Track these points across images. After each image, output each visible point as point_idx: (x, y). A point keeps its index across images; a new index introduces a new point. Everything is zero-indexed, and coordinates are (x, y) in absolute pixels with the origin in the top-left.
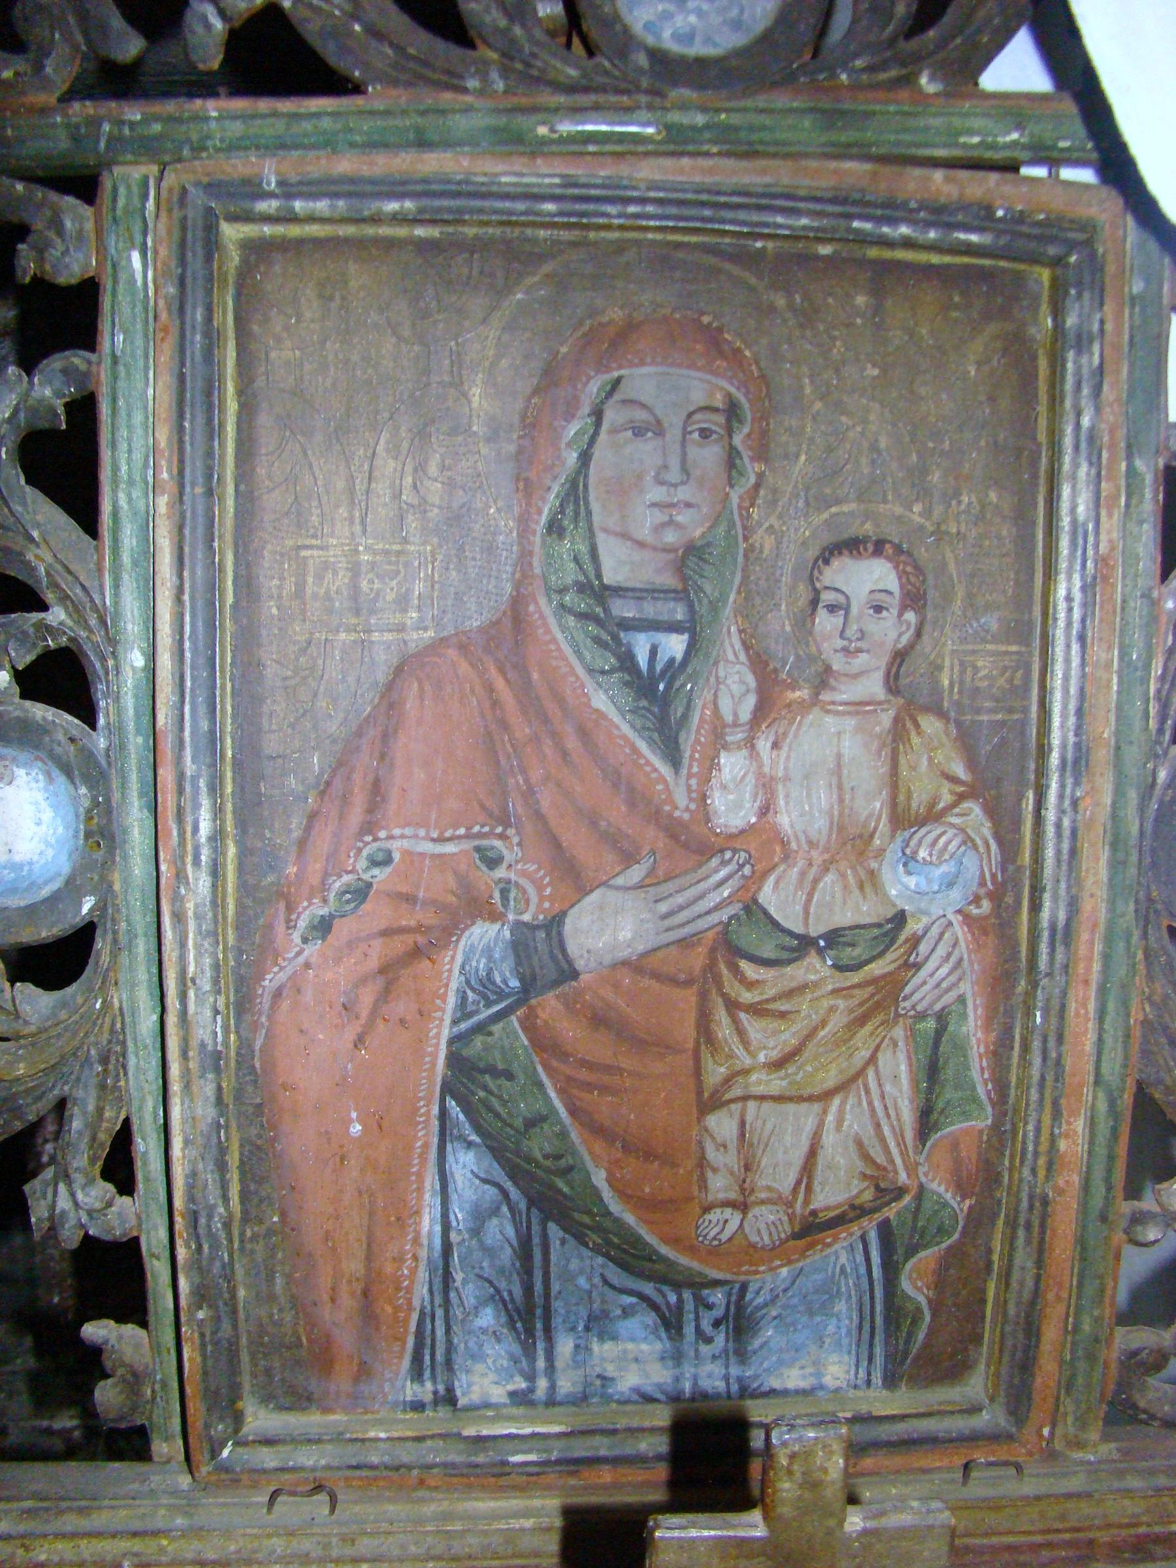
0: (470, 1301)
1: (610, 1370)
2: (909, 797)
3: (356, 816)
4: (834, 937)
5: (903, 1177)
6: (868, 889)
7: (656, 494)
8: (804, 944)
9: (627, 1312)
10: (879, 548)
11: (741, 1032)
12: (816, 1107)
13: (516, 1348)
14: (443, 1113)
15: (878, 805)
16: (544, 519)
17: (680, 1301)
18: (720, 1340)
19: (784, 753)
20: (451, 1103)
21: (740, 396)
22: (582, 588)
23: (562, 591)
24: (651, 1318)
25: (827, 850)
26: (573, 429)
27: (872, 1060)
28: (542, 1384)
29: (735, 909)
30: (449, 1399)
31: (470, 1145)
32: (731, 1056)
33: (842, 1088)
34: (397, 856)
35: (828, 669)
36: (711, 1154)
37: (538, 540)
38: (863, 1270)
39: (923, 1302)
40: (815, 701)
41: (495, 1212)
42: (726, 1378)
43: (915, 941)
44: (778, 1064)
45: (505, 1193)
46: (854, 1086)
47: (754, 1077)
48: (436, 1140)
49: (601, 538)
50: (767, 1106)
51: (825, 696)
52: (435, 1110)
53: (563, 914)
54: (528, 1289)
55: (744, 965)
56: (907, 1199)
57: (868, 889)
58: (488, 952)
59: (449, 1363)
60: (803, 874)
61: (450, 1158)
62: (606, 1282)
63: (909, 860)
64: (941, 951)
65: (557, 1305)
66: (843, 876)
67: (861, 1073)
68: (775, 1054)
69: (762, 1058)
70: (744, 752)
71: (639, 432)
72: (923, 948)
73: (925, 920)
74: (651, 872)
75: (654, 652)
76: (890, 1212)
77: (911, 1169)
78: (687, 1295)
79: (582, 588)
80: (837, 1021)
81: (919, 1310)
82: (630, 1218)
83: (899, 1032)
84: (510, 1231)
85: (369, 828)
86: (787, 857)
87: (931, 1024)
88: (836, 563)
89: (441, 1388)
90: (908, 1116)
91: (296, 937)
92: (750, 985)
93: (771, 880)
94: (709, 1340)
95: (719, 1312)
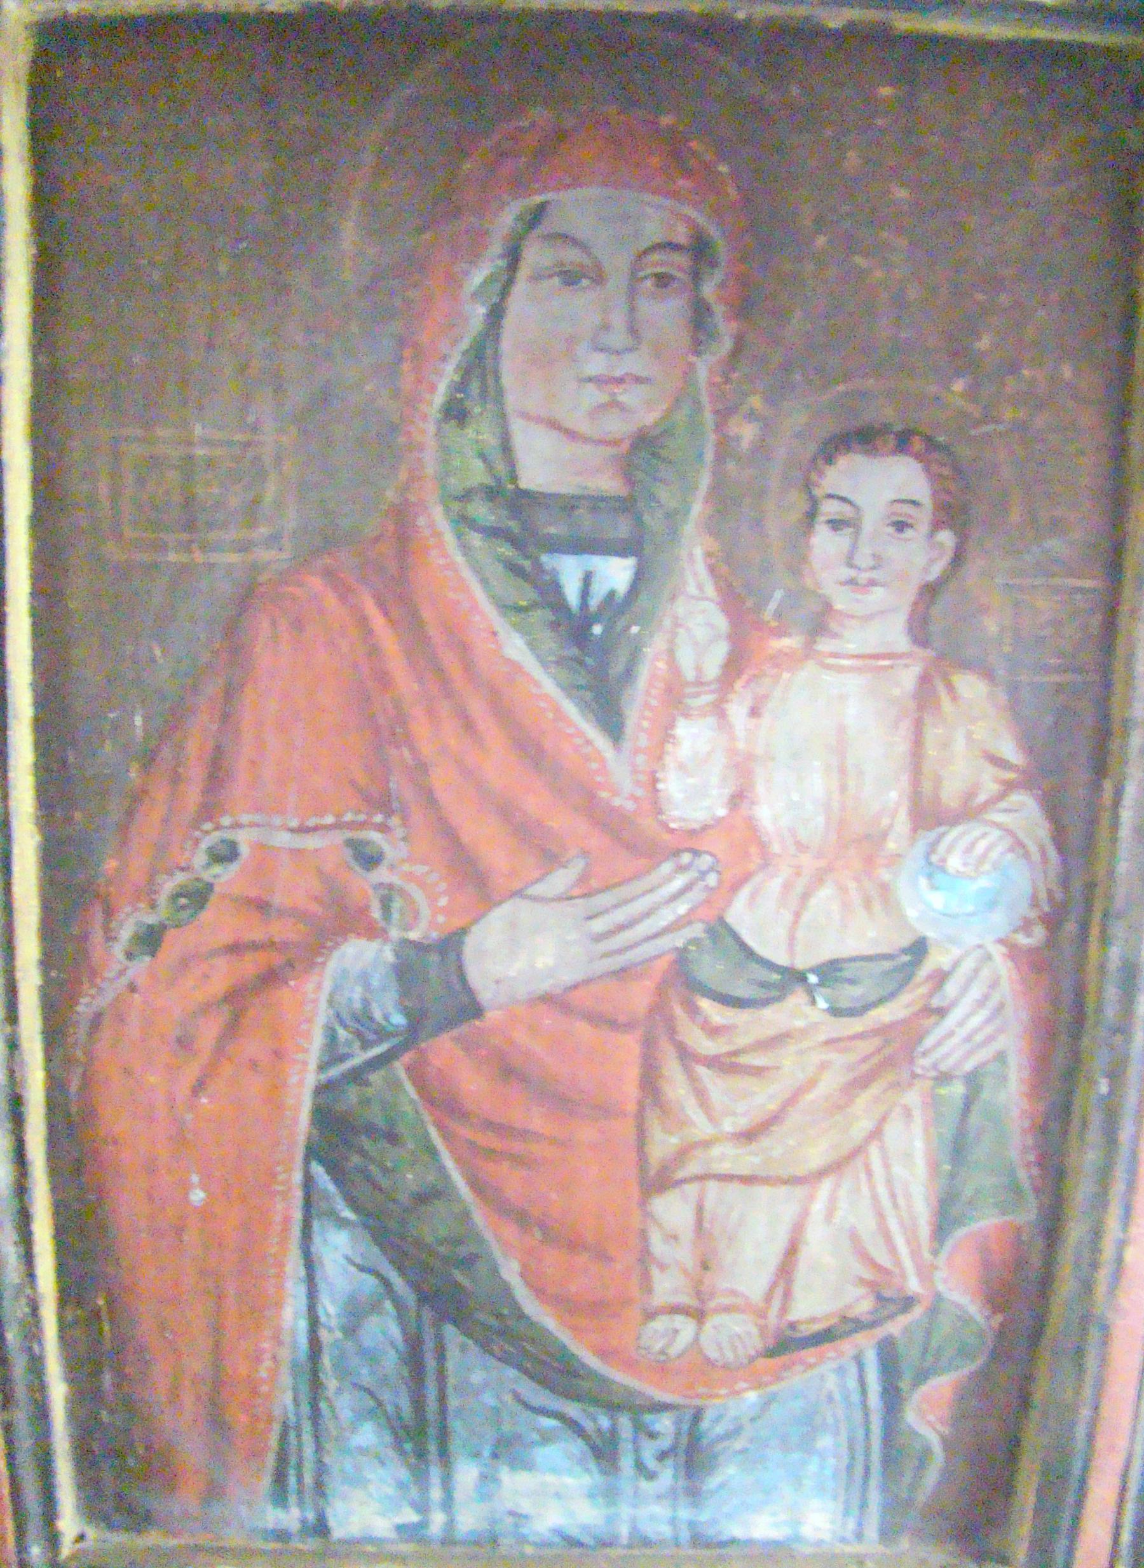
0: (346, 1415)
1: (525, 1506)
2: (938, 781)
3: (193, 795)
4: (830, 971)
5: (913, 1285)
6: (877, 907)
7: (596, 365)
8: (794, 977)
9: (546, 1438)
10: (903, 443)
11: (701, 1095)
12: (799, 1191)
13: (404, 1474)
14: (308, 1181)
15: (893, 795)
16: (439, 398)
17: (614, 1431)
18: (667, 1476)
19: (766, 720)
20: (317, 1169)
21: (713, 231)
22: (492, 494)
23: (466, 496)
24: (578, 1446)
25: (819, 855)
26: (478, 277)
27: (876, 1134)
28: (438, 1519)
29: (697, 930)
30: (321, 1528)
31: (342, 1223)
32: (685, 1123)
33: (835, 1168)
34: (244, 850)
35: (828, 607)
36: (658, 1245)
37: (432, 428)
38: (856, 1398)
39: (934, 1440)
40: (809, 652)
41: (375, 1307)
42: (673, 1522)
43: (940, 978)
44: (748, 1136)
45: (386, 1283)
46: (859, 1162)
47: (716, 1151)
48: (298, 1216)
49: (517, 426)
50: (735, 1187)
51: (825, 645)
52: (298, 1177)
53: (464, 931)
54: (418, 1403)
55: (705, 1004)
56: (917, 1311)
57: (877, 907)
58: (364, 978)
59: (320, 1488)
60: (787, 887)
61: (317, 1239)
62: (517, 1397)
63: (934, 868)
64: (975, 992)
65: (456, 1425)
66: (843, 890)
67: (857, 1152)
68: (743, 1123)
69: (728, 1126)
70: (711, 720)
71: (570, 278)
72: (951, 988)
73: (956, 952)
74: (583, 879)
75: (587, 579)
76: (894, 1328)
77: (925, 1273)
78: (625, 1423)
79: (492, 494)
80: (829, 1084)
81: (927, 1451)
82: (550, 1322)
83: (913, 1098)
84: (395, 1331)
85: (208, 812)
86: (767, 860)
87: (958, 1089)
88: (842, 462)
89: (311, 1516)
90: (922, 1211)
91: (118, 950)
92: (714, 1031)
93: (745, 892)
94: (652, 1476)
95: (666, 1443)
